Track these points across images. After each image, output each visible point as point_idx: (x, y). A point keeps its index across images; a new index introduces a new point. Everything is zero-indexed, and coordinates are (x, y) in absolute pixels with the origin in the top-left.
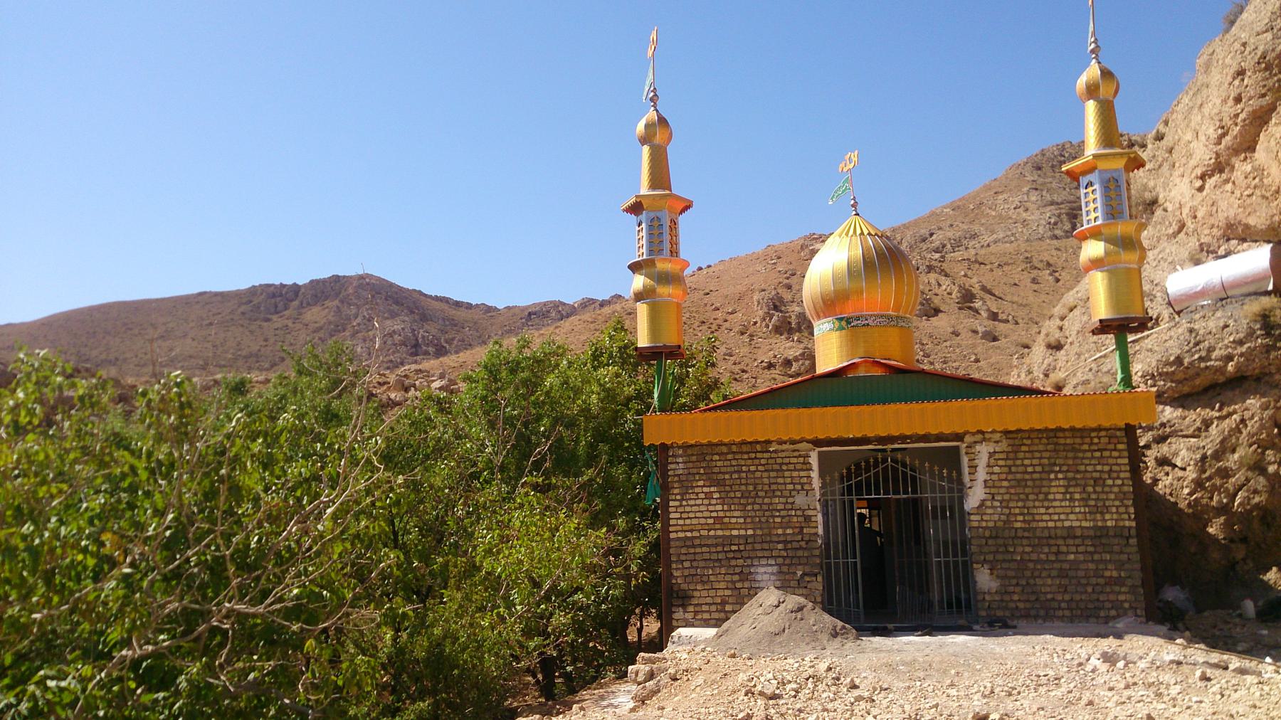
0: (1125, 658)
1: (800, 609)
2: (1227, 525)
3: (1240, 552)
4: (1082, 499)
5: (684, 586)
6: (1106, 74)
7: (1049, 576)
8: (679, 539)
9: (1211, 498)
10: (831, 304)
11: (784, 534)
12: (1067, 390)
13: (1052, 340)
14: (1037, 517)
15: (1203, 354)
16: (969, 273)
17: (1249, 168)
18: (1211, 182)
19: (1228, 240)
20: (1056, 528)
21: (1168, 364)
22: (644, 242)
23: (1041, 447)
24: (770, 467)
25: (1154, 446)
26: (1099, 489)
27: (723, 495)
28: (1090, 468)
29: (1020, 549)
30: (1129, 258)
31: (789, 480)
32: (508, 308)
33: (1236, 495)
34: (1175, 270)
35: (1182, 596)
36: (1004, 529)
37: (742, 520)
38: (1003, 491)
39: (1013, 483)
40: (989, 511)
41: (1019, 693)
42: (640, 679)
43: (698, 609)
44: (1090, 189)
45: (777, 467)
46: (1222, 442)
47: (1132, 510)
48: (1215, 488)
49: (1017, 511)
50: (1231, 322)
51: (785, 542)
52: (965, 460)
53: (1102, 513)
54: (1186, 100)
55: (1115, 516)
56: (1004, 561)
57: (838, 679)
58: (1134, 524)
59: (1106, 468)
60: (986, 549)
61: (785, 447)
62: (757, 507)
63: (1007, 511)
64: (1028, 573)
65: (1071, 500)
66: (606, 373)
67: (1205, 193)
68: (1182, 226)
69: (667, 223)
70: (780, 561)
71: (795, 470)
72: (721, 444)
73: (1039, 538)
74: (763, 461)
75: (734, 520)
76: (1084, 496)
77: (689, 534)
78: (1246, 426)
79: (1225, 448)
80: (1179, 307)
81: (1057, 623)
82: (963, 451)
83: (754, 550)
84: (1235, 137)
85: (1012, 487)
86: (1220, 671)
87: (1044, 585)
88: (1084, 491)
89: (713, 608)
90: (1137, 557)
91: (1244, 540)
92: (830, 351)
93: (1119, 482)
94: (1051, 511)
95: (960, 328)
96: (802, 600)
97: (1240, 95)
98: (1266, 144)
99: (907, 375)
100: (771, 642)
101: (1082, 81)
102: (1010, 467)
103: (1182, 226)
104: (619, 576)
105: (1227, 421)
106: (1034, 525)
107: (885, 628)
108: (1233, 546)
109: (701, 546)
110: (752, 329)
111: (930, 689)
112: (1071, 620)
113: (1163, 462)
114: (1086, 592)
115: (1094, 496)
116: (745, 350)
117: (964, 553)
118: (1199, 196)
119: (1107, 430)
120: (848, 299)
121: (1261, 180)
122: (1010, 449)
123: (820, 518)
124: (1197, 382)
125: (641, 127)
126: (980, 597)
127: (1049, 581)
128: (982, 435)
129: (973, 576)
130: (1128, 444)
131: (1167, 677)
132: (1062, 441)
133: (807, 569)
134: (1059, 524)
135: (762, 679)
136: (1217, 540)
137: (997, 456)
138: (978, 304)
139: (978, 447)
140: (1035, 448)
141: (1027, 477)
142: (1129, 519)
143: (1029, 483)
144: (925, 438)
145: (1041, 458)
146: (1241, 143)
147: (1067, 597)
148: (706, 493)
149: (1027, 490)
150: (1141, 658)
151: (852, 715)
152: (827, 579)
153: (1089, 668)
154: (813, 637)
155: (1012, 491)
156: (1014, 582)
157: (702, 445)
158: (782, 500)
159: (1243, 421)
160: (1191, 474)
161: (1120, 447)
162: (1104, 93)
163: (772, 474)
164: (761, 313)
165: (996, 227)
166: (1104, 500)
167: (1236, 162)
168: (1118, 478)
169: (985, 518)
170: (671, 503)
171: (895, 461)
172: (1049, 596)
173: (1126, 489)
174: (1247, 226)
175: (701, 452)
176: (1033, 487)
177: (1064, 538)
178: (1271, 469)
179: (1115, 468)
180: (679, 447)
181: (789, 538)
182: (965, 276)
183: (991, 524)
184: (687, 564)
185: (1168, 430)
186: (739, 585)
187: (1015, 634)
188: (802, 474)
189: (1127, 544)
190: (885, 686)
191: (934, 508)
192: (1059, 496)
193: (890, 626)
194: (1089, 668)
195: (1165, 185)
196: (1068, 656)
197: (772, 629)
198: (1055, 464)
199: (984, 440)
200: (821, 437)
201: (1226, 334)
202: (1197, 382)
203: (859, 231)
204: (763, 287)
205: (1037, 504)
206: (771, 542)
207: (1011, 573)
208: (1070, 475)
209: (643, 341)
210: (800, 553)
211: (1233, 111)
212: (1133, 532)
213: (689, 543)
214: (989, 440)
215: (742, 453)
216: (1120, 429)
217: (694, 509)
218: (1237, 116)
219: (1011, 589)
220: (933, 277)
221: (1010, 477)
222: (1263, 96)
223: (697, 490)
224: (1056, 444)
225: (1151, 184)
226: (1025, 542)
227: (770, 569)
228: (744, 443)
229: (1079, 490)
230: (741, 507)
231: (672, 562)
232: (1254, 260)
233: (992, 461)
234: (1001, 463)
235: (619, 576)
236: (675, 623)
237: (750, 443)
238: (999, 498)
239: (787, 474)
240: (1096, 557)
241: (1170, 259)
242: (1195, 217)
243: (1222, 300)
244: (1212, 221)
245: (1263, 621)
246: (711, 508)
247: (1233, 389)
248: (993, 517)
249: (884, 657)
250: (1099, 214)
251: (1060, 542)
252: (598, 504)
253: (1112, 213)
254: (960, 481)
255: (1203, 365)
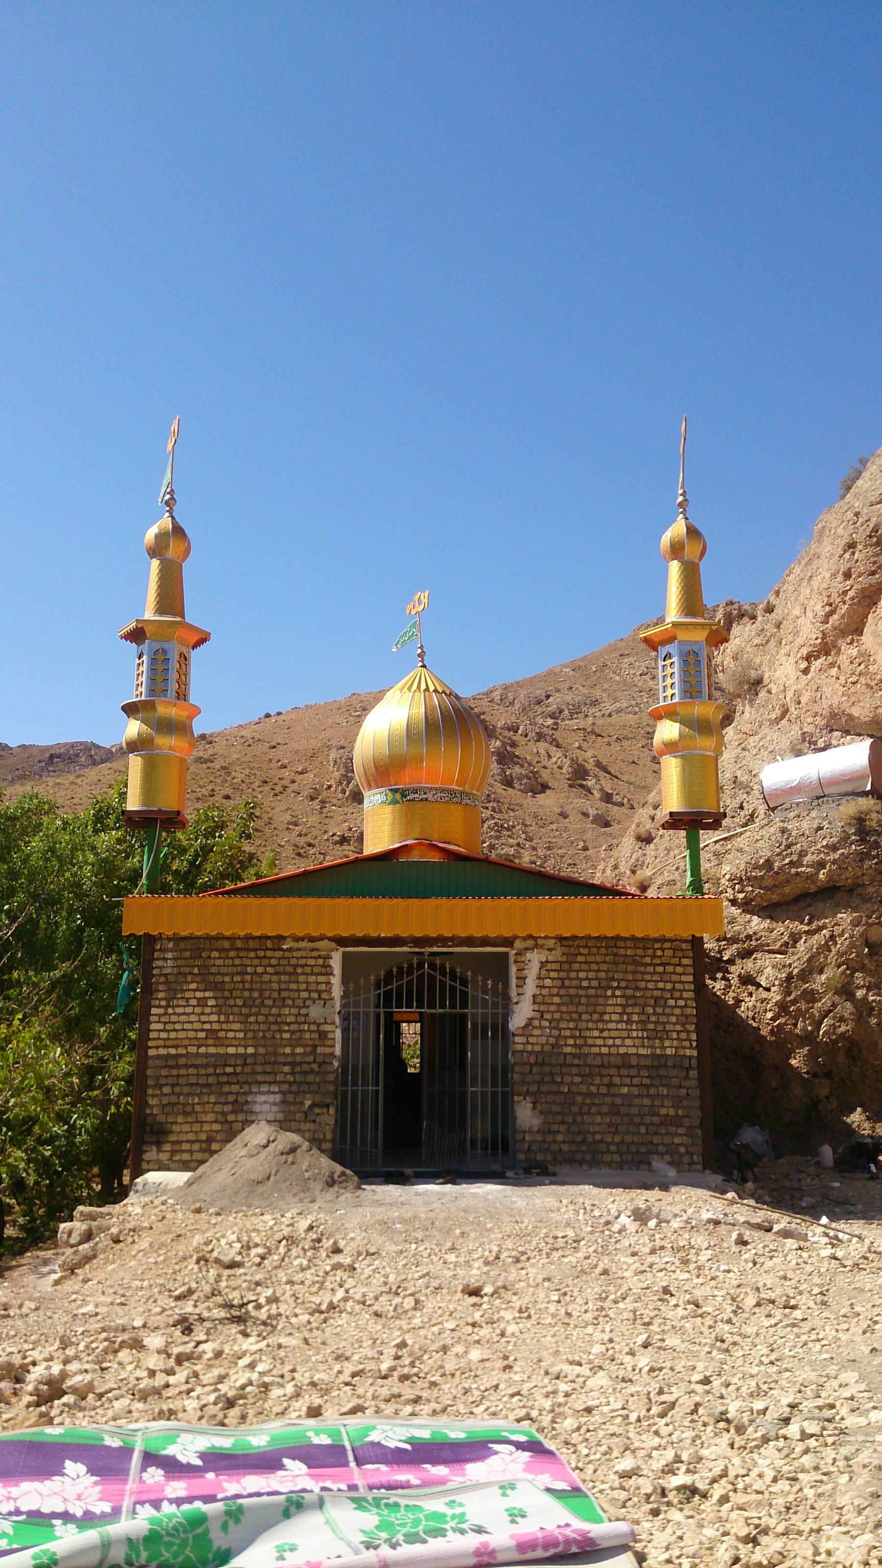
0: (657, 1216)
1: (293, 1150)
2: (811, 1058)
3: (823, 1089)
4: (640, 1022)
5: (161, 1118)
6: (692, 532)
7: (599, 1113)
8: (158, 1057)
9: (795, 1025)
10: (385, 771)
11: (293, 1054)
12: (651, 893)
13: (642, 831)
14: (590, 1042)
15: (795, 858)
16: (585, 745)
17: (855, 652)
18: (816, 664)
19: (831, 731)
20: (609, 1054)
21: (756, 867)
22: (144, 679)
23: (599, 958)
24: (281, 969)
25: (738, 961)
26: (659, 1010)
27: (220, 1002)
28: (651, 985)
29: (568, 1079)
30: (705, 743)
31: (303, 986)
32: (24, 747)
33: (821, 1022)
34: (775, 760)
35: (760, 1139)
36: (551, 1054)
37: (241, 1035)
38: (553, 1008)
39: (565, 999)
40: (537, 1032)
41: (529, 1259)
42: (72, 1241)
43: (176, 1147)
44: (668, 662)
45: (289, 969)
46: (809, 960)
47: (694, 1036)
48: (800, 1013)
49: (568, 1033)
50: (825, 824)
51: (293, 1064)
52: (513, 969)
53: (661, 1039)
54: (797, 570)
55: (675, 1043)
56: (550, 1093)
57: (319, 1241)
58: (695, 1053)
59: (669, 986)
60: (529, 1078)
61: (302, 944)
62: (261, 1018)
63: (556, 1033)
64: (575, 1109)
65: (629, 1022)
66: (106, 840)
67: (809, 676)
68: (785, 712)
69: (174, 657)
70: (285, 1087)
71: (312, 974)
72: (220, 938)
73: (590, 1066)
74: (273, 962)
75: (231, 1035)
76: (643, 1018)
77: (173, 1051)
78: (836, 943)
79: (812, 968)
80: (774, 803)
81: (605, 1170)
82: (512, 959)
83: (254, 1073)
84: (843, 617)
85: (563, 1004)
86: (761, 1233)
87: (592, 1123)
88: (643, 1013)
89: (196, 1147)
90: (696, 1093)
91: (828, 1075)
92: (380, 828)
93: (682, 1003)
94: (606, 1034)
95: (568, 809)
96: (295, 1138)
97: (849, 569)
98: (873, 627)
99: (469, 864)
100: (251, 1192)
101: (667, 538)
102: (563, 980)
103: (785, 712)
104: (94, 1102)
105: (816, 937)
106: (586, 1050)
107: (402, 1174)
108: (816, 1081)
109: (187, 1066)
110: (325, 794)
111: (425, 1254)
112: (620, 1166)
113: (747, 980)
114: (639, 1133)
115: (653, 1019)
116: (313, 819)
117: (505, 1084)
118: (804, 679)
119: (671, 940)
120: (405, 766)
121: (866, 667)
122: (564, 959)
123: (338, 1034)
124: (787, 890)
125: (151, 533)
126: (519, 1137)
127: (599, 1119)
128: (534, 941)
129: (513, 1111)
130: (693, 958)
131: (700, 1240)
132: (622, 952)
133: (318, 1098)
134: (613, 1050)
135: (223, 1242)
136: (799, 1074)
137: (549, 967)
138: (590, 783)
139: (529, 955)
140: (591, 958)
141: (582, 992)
142: (691, 1047)
143: (583, 1000)
144: (469, 941)
145: (598, 971)
146: (847, 625)
147: (617, 1139)
148: (199, 999)
149: (581, 1009)
150: (676, 1216)
151: (320, 1289)
152: (341, 1113)
153: (616, 1227)
154: (304, 1185)
155: (564, 1009)
156: (559, 1118)
157: (198, 938)
158: (294, 1011)
159: (832, 937)
160: (775, 996)
161: (685, 961)
162: (690, 551)
163: (284, 978)
164: (337, 775)
165: (619, 694)
166: (664, 1023)
167: (842, 644)
168: (681, 998)
169: (531, 1040)
170: (154, 1011)
171: (432, 966)
172: (598, 1137)
173: (688, 1011)
174: (851, 717)
175: (195, 947)
176: (587, 1005)
177: (618, 1068)
178: (860, 994)
179: (678, 986)
180: (169, 939)
181: (298, 1059)
182: (579, 748)
183: (537, 1048)
184: (167, 1090)
185: (754, 943)
186: (231, 1118)
187: (552, 1183)
188: (321, 979)
189: (687, 1077)
190: (373, 1250)
191: (475, 1025)
192: (615, 1017)
193: (408, 1171)
194: (616, 1227)
195: (771, 664)
196: (597, 1213)
197: (254, 1176)
198: (613, 979)
199: (536, 946)
200: (345, 935)
201: (817, 839)
202: (787, 890)
203: (423, 687)
204: (342, 743)
205: (590, 1025)
206: (276, 1063)
207: (555, 1108)
208: (629, 992)
209: (133, 804)
210: (310, 1078)
211: (841, 587)
212: (694, 1062)
213: (171, 1062)
214: (542, 946)
215: (248, 950)
216: (686, 941)
217: (182, 1018)
218: (845, 593)
219: (555, 1127)
220: (542, 746)
221: (562, 992)
222: (873, 573)
223: (188, 995)
224: (615, 955)
225: (758, 661)
226: (574, 1070)
227: (271, 1098)
228: (249, 937)
229: (637, 1010)
230: (241, 1019)
231: (147, 1086)
232: (853, 756)
233: (543, 972)
234: (553, 974)
235: (94, 1102)
236: (144, 1166)
237: (259, 938)
238: (549, 1016)
239: (302, 978)
240: (652, 1091)
241: (771, 748)
242: (799, 703)
243: (818, 798)
244: (816, 708)
245: (840, 1171)
246: (204, 1018)
247: (824, 900)
248: (539, 1040)
249: (381, 1213)
250: (676, 691)
251: (614, 1072)
252: (74, 1008)
253: (691, 690)
254: (506, 997)
255: (793, 871)
